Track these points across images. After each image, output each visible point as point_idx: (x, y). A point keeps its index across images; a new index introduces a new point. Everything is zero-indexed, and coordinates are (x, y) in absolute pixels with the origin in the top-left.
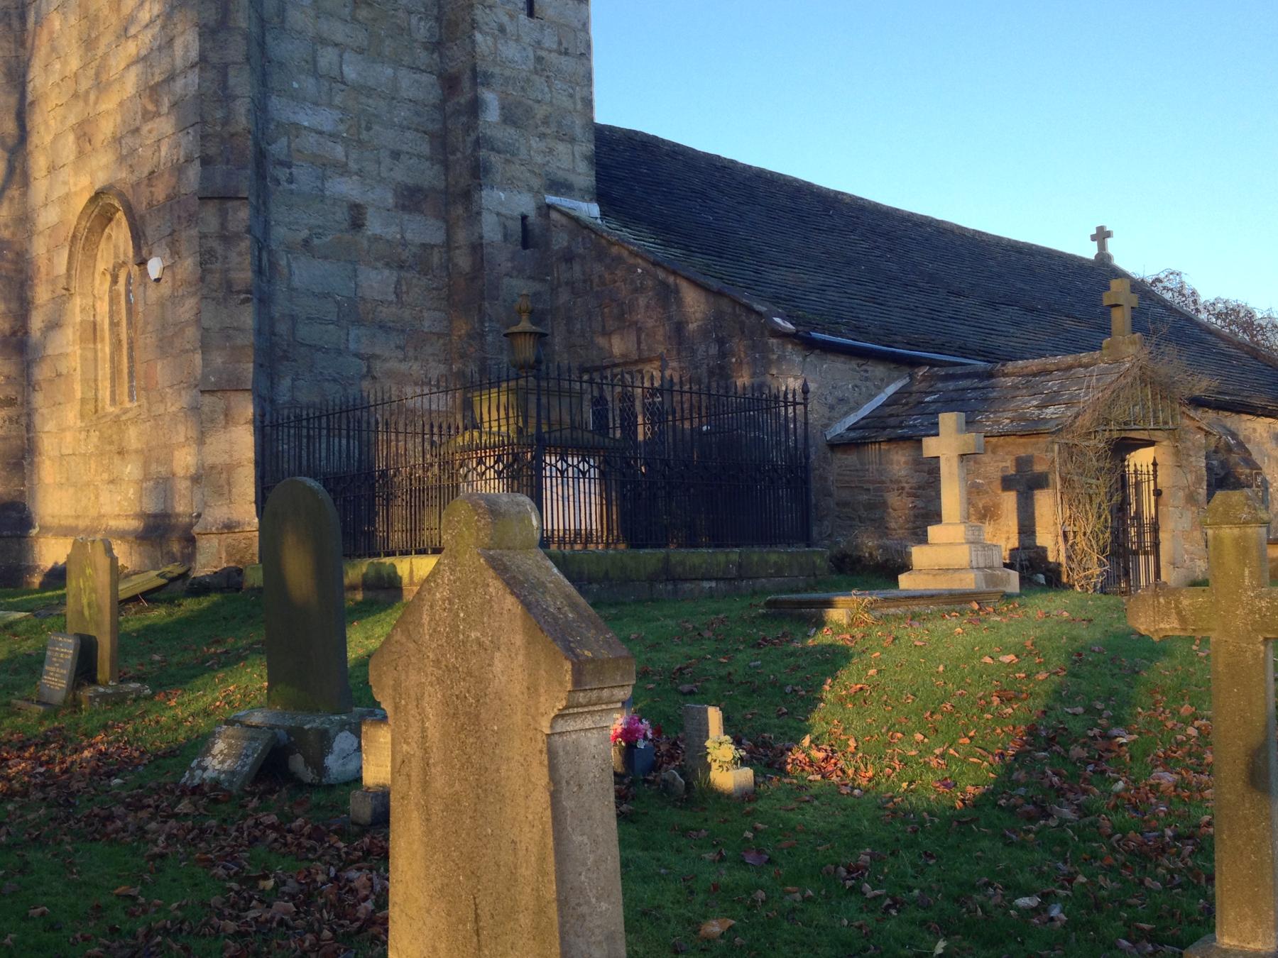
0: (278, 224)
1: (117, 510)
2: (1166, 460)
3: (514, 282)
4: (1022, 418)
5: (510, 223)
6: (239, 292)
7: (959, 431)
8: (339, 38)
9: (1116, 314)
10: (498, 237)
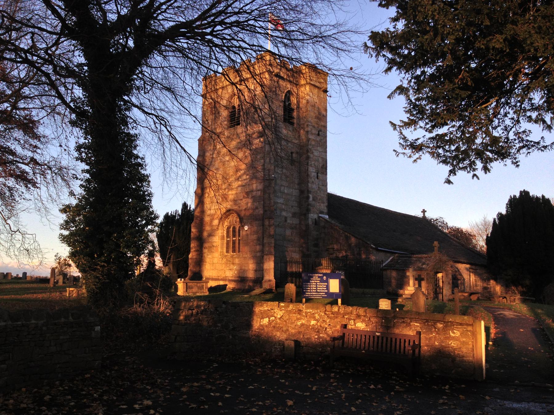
1: (231, 276)
2: (444, 276)
4: (419, 267)
7: (413, 271)
8: (284, 185)
9: (435, 248)
10: (311, 223)
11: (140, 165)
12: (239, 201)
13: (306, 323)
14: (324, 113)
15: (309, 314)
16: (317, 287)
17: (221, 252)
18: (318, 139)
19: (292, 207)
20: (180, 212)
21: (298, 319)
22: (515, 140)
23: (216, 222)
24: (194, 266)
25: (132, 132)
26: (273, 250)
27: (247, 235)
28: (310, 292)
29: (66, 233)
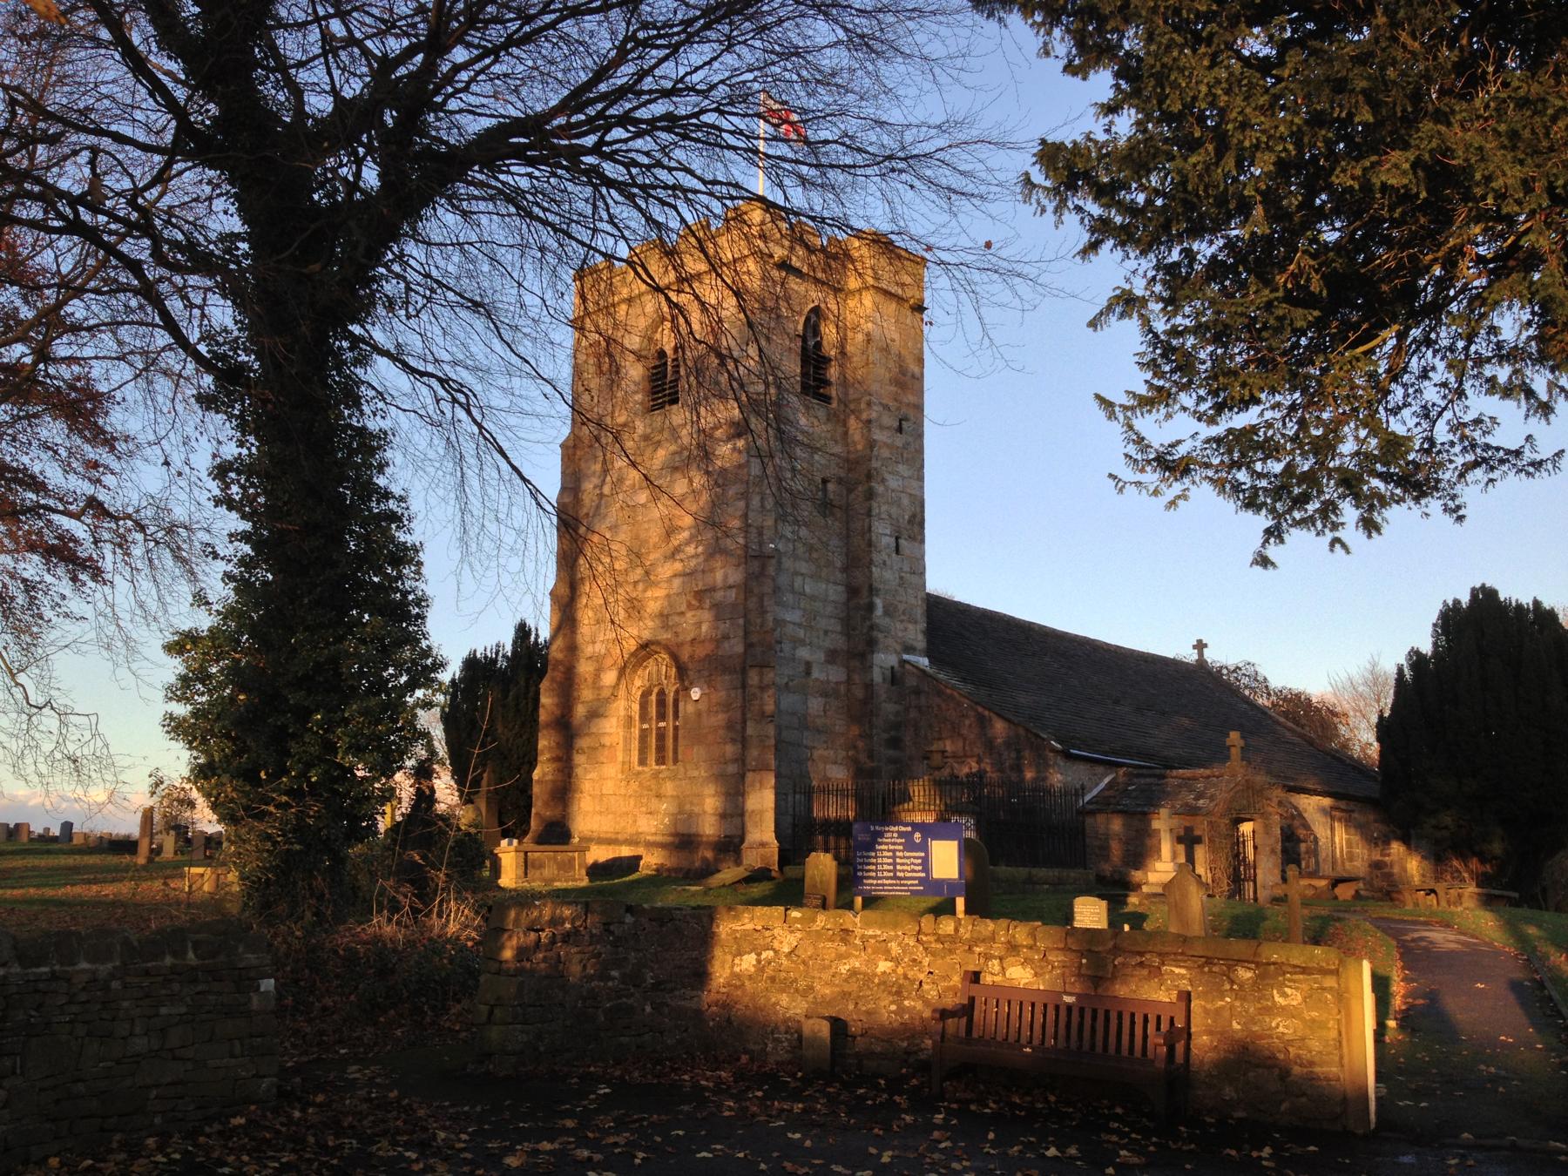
1: (653, 830)
2: (1260, 830)
4: (1187, 804)
9: (1233, 750)
11: (394, 517)
12: (677, 619)
13: (864, 968)
14: (916, 370)
15: (873, 941)
16: (895, 864)
17: (624, 763)
18: (899, 441)
19: (826, 632)
20: (509, 649)
21: (840, 957)
22: (1452, 444)
23: (609, 678)
24: (546, 804)
25: (373, 425)
26: (771, 758)
27: (699, 714)
28: (877, 878)
29: (181, 710)
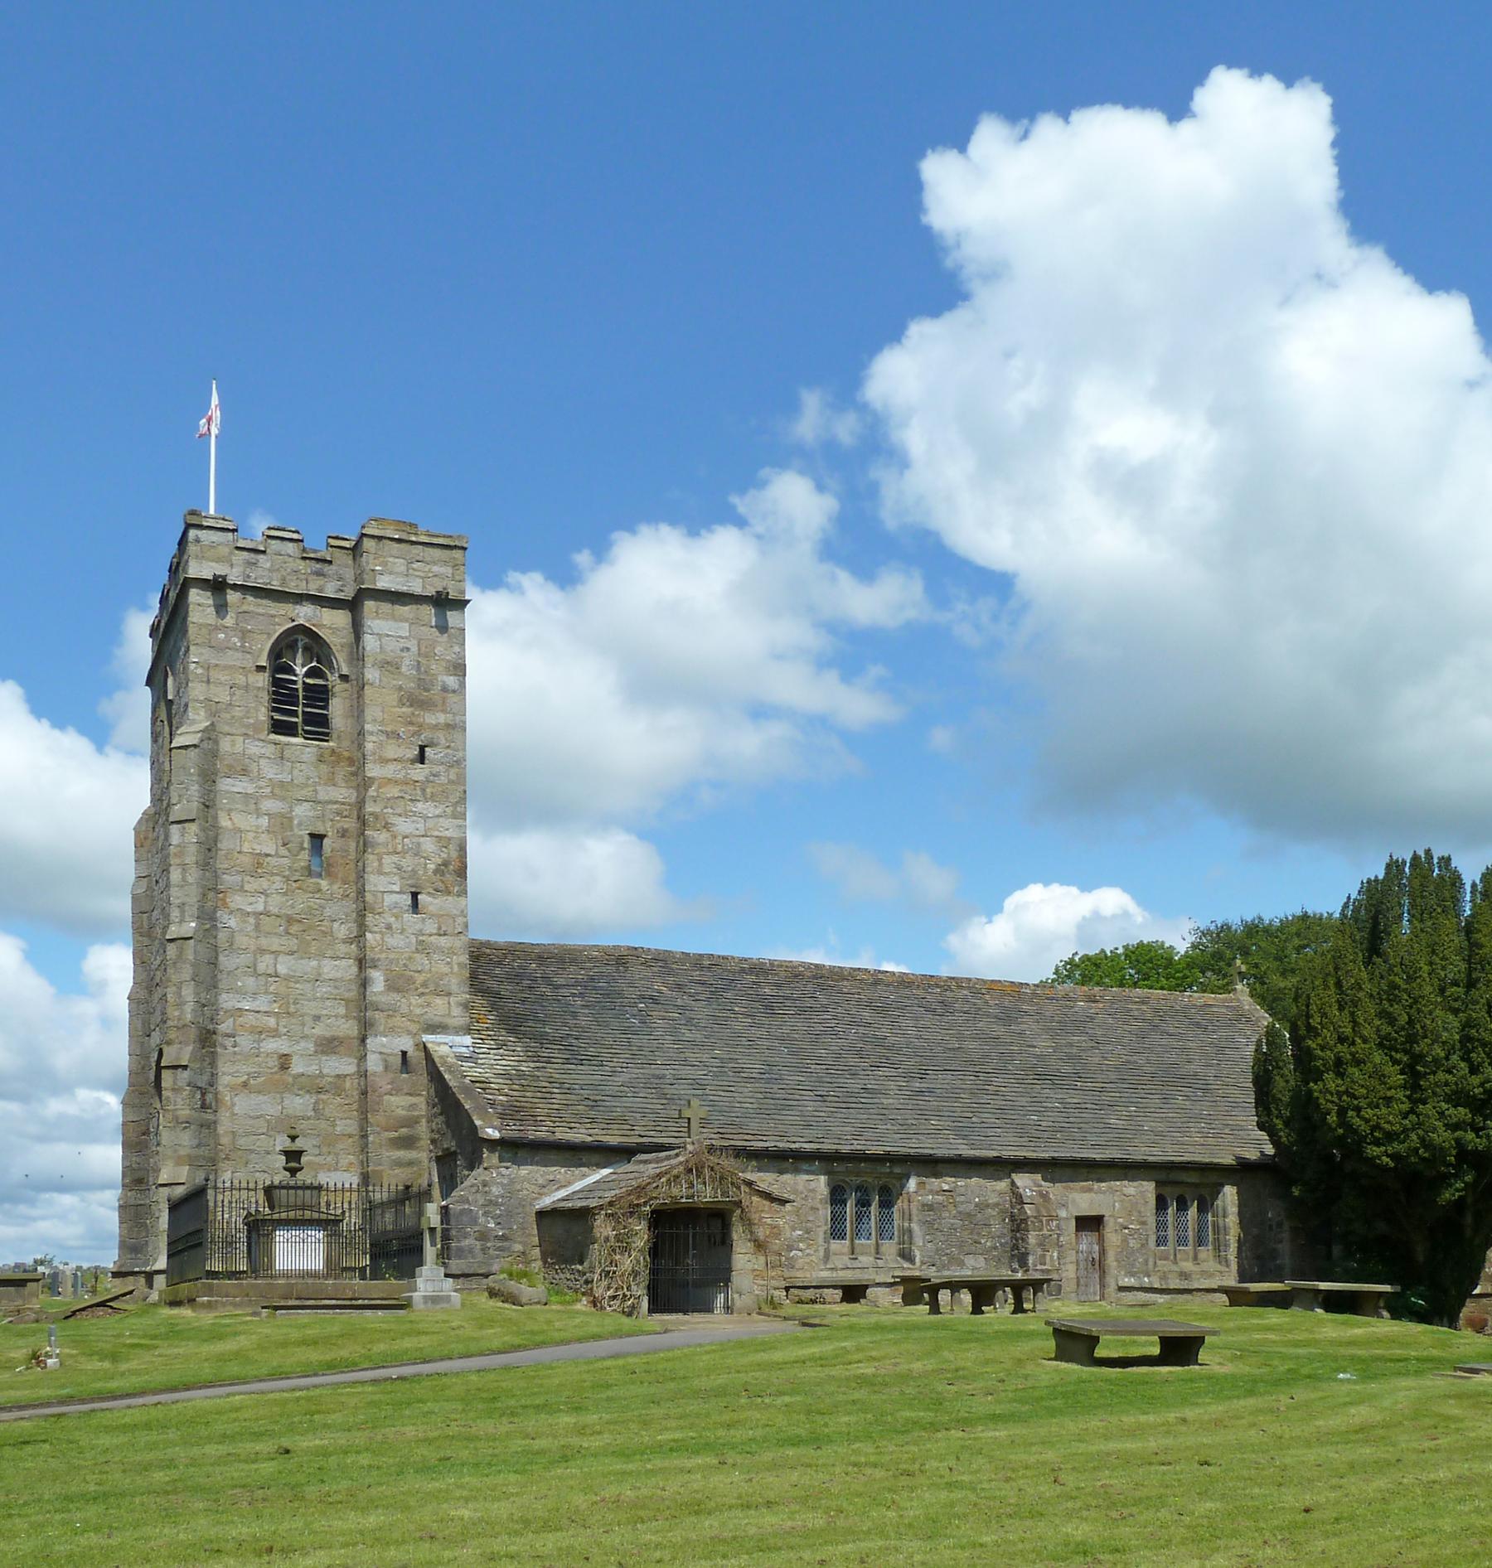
0: (224, 1074)
3: (393, 1099)
5: (391, 1059)
6: (182, 1123)
10: (380, 1068)
14: (451, 681)
18: (419, 772)
